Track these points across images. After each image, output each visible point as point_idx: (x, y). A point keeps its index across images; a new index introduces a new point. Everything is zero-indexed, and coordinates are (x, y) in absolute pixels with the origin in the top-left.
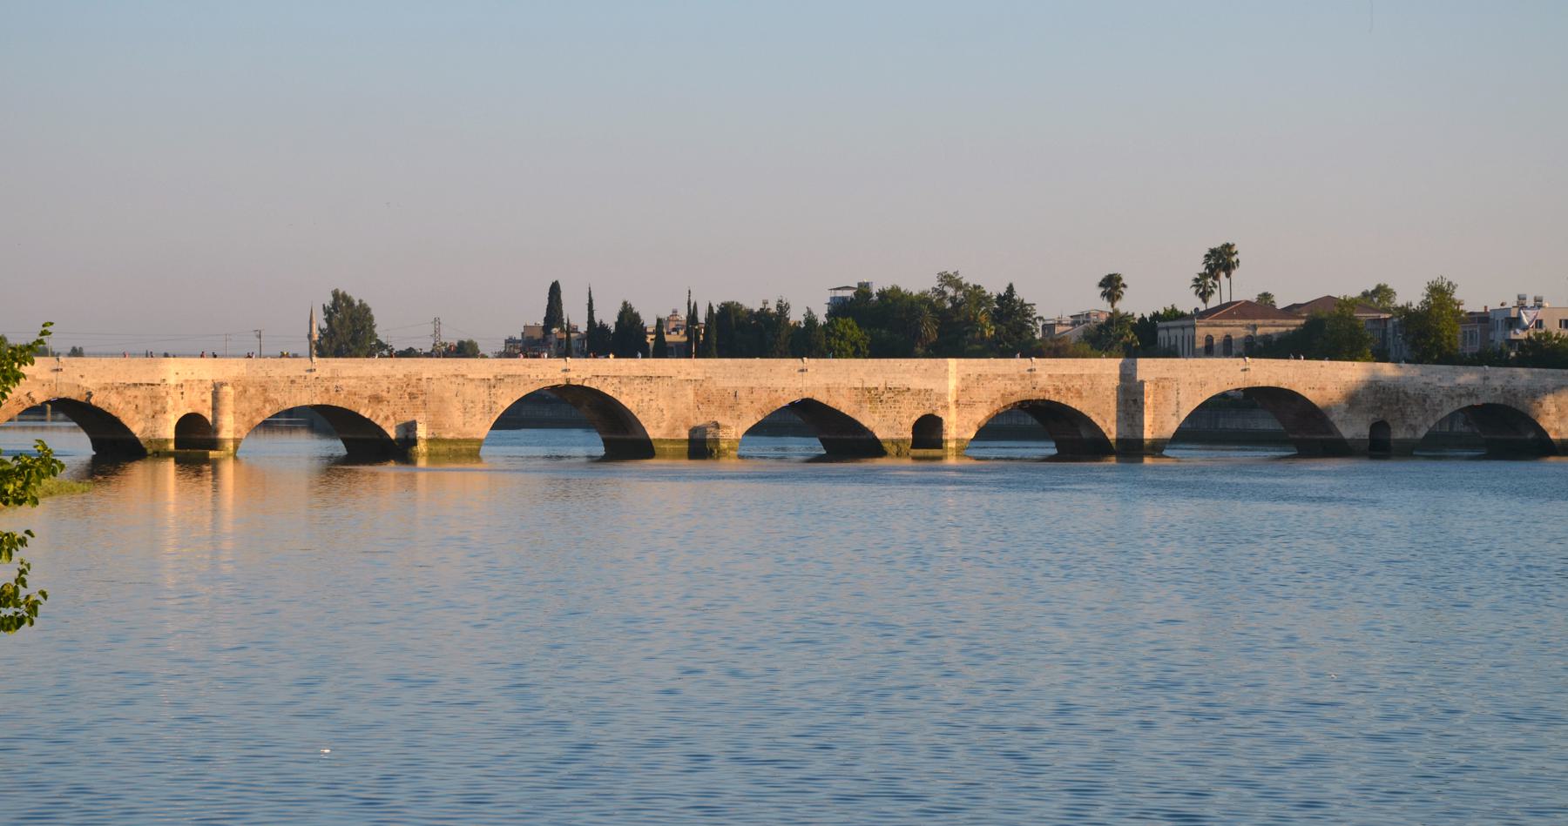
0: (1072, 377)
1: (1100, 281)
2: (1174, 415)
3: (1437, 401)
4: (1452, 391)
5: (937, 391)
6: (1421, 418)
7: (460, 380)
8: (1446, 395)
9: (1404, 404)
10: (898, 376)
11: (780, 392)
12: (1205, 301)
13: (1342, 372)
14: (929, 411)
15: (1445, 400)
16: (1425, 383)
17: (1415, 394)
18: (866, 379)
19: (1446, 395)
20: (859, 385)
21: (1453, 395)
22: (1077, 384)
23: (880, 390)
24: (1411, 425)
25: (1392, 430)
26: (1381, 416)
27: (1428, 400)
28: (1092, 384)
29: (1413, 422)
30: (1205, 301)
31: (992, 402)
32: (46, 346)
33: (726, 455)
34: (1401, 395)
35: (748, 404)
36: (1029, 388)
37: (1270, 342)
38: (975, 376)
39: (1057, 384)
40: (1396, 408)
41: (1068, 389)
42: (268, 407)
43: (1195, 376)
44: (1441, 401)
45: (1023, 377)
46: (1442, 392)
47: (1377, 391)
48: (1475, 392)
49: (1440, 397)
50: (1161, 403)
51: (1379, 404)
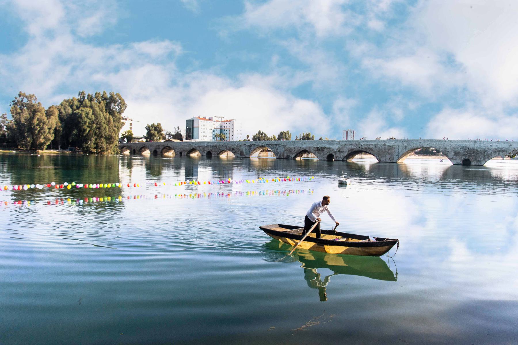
0: (370, 145)
1: (150, 124)
2: (397, 155)
3: (489, 153)
4: (496, 150)
5: (332, 148)
6: (482, 158)
7: (245, 145)
8: (494, 151)
9: (476, 154)
10: (324, 144)
11: (300, 148)
12: (248, 138)
13: (452, 143)
14: (330, 153)
15: (493, 152)
16: (485, 147)
17: (480, 150)
18: (317, 145)
19: (494, 151)
20: (315, 146)
21: (496, 151)
22: (371, 147)
23: (320, 148)
24: (479, 161)
25: (471, 162)
26: (467, 157)
27: (486, 152)
28: (376, 146)
29: (480, 160)
30: (248, 138)
31: (348, 151)
32: (257, 133)
33: (272, 167)
34: (475, 151)
35: (294, 151)
36: (358, 147)
37: (267, 161)
38: (344, 144)
39: (365, 146)
40: (473, 155)
41: (369, 148)
42: (219, 150)
43: (404, 144)
44: (491, 153)
45: (357, 145)
46: (491, 150)
47: (466, 149)
48: (506, 150)
49: (491, 152)
50: (393, 152)
51: (466, 153)
